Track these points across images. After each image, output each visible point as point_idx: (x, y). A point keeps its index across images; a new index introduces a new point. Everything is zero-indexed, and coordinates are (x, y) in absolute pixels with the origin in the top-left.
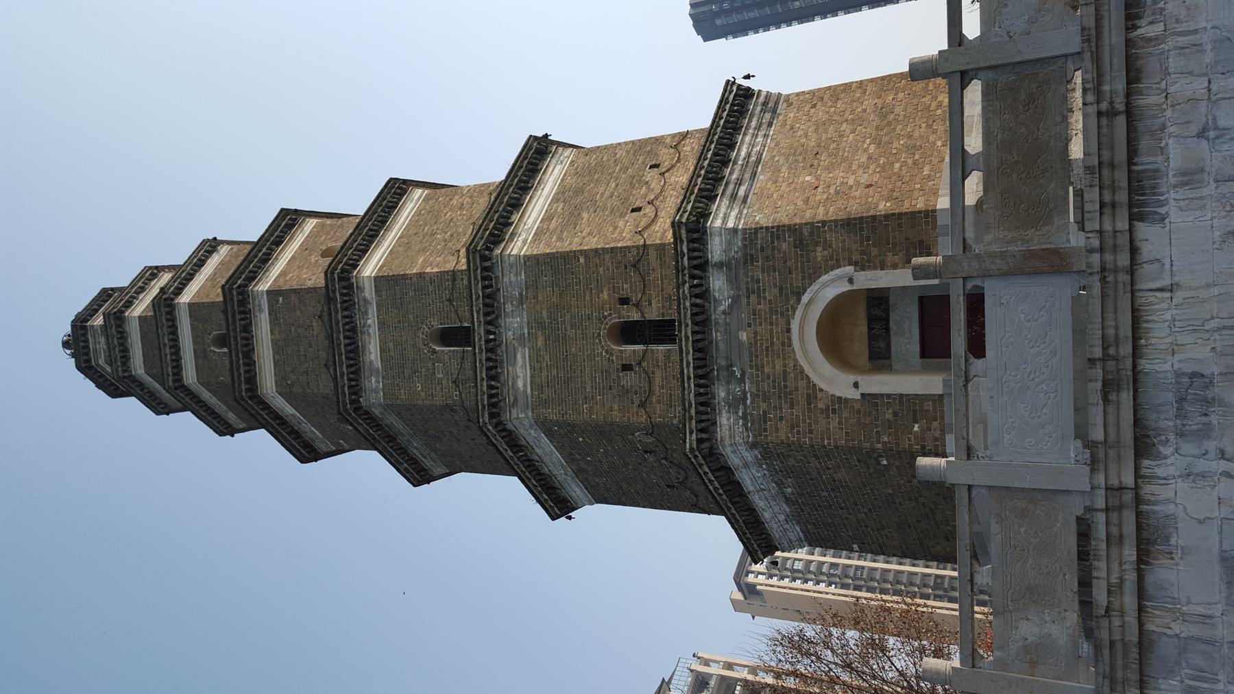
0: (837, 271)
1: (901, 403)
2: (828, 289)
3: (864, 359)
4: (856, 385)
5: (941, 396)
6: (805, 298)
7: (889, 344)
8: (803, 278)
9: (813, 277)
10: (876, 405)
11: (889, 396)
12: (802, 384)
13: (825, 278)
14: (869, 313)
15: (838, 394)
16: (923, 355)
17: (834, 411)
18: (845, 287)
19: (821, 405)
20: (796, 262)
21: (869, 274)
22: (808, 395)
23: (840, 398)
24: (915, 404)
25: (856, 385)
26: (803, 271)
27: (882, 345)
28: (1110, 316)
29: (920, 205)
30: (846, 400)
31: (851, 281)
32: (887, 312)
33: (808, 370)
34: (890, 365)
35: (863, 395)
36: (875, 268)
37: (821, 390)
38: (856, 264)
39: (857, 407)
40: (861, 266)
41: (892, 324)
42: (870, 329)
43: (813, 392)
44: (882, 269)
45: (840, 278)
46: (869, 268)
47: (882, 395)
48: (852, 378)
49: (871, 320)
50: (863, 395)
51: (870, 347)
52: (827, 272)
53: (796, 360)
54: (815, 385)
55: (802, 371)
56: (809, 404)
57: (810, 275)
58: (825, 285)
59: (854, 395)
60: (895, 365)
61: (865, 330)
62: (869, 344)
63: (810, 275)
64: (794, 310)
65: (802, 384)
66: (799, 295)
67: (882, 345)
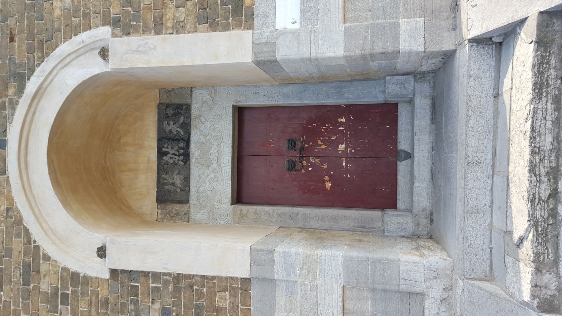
0: (85, 37)
1: (177, 290)
2: (69, 70)
3: (148, 203)
4: (102, 252)
5: (246, 281)
6: (31, 86)
7: (187, 180)
8: (30, 50)
9: (44, 47)
10: (134, 291)
11: (156, 276)
12: (18, 245)
13: (65, 48)
14: (160, 130)
15: (74, 267)
16: (239, 197)
17: (65, 297)
18: (95, 67)
19: (45, 287)
20: (21, 21)
21: (135, 40)
22: (27, 266)
23: (75, 276)
24: (200, 294)
25: (102, 252)
26: (31, 36)
27: (178, 180)
28: (44, 225)
29: (256, 24)
30: (87, 280)
31: (104, 53)
32: (186, 127)
33: (29, 220)
34: (187, 214)
35: (114, 272)
36: (146, 30)
37: (47, 258)
38: (115, 23)
39: (104, 293)
40: (123, 26)
41: (193, 146)
42: (161, 154)
43: (34, 258)
44: (158, 33)
45: (86, 49)
46: (136, 30)
47: (146, 274)
48: (98, 238)
49: (163, 139)
50: (114, 272)
51: (160, 183)
52: (68, 37)
53: (10, 200)
54: (37, 247)
55: (19, 221)
56: (26, 283)
57: (41, 43)
58: (65, 62)
59: (99, 270)
60: (194, 215)
61: (153, 155)
62: (159, 178)
63: (41, 43)
64: (13, 105)
65: (18, 245)
66: (21, 79)
67: (178, 180)
